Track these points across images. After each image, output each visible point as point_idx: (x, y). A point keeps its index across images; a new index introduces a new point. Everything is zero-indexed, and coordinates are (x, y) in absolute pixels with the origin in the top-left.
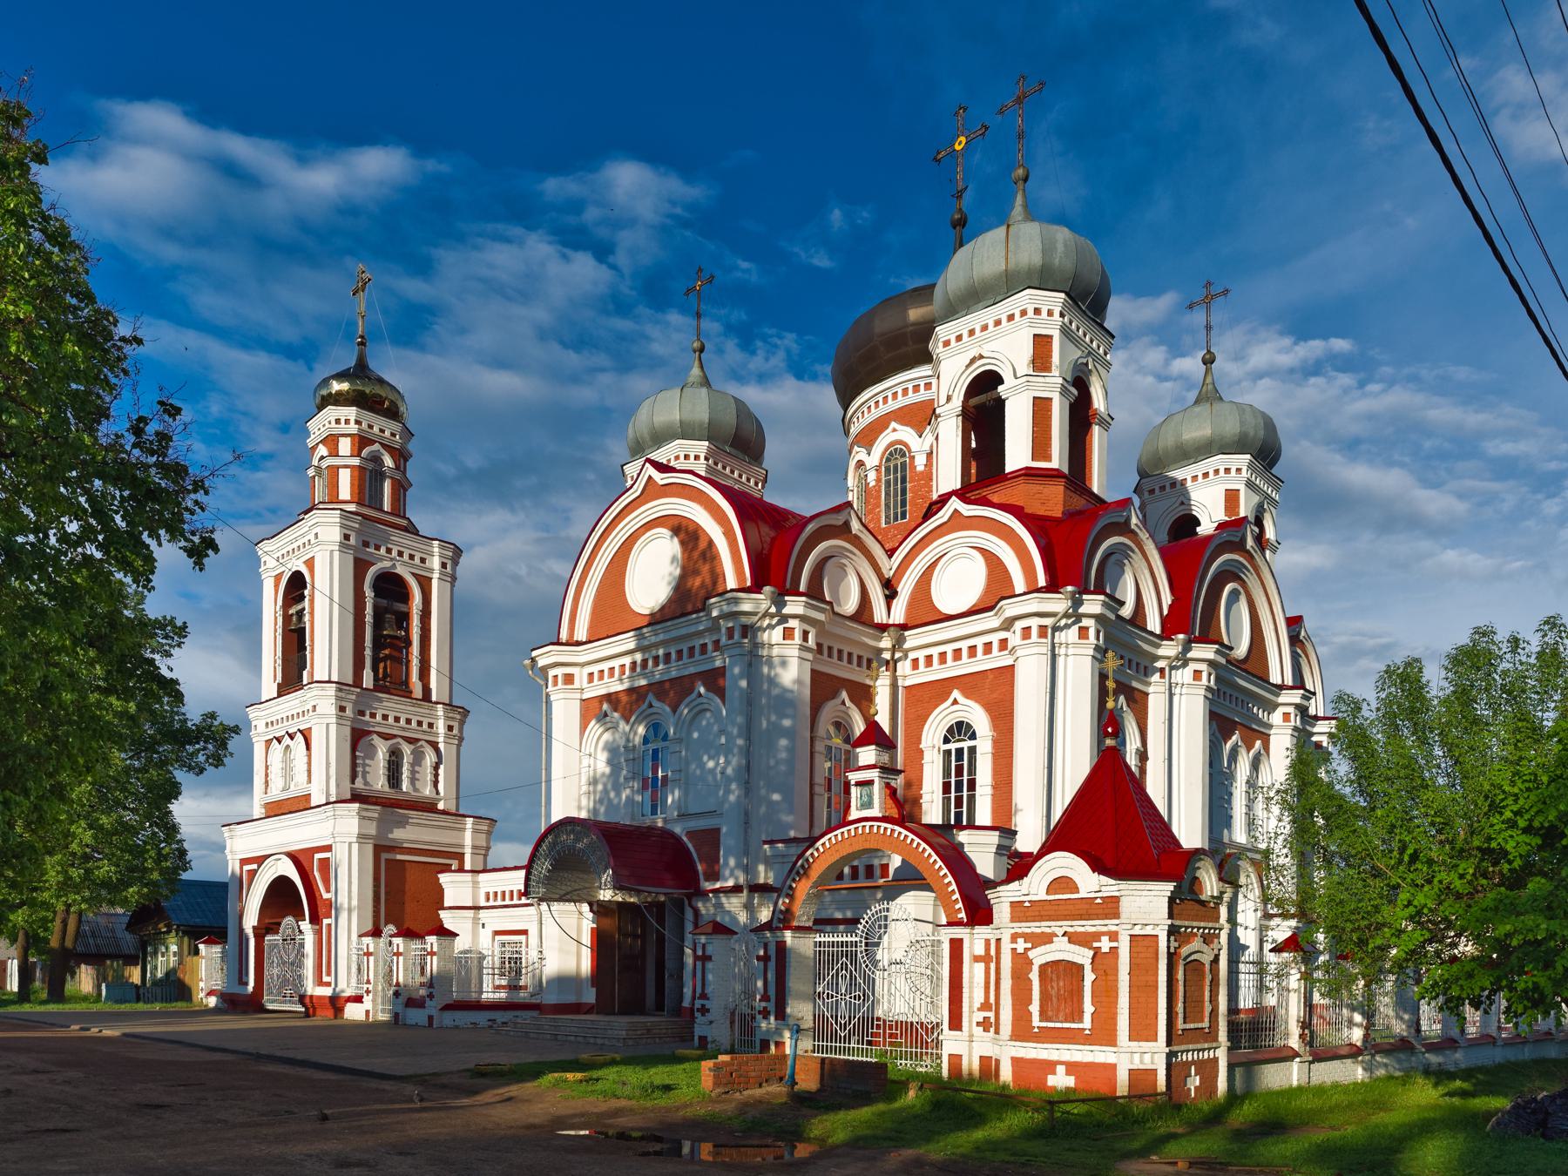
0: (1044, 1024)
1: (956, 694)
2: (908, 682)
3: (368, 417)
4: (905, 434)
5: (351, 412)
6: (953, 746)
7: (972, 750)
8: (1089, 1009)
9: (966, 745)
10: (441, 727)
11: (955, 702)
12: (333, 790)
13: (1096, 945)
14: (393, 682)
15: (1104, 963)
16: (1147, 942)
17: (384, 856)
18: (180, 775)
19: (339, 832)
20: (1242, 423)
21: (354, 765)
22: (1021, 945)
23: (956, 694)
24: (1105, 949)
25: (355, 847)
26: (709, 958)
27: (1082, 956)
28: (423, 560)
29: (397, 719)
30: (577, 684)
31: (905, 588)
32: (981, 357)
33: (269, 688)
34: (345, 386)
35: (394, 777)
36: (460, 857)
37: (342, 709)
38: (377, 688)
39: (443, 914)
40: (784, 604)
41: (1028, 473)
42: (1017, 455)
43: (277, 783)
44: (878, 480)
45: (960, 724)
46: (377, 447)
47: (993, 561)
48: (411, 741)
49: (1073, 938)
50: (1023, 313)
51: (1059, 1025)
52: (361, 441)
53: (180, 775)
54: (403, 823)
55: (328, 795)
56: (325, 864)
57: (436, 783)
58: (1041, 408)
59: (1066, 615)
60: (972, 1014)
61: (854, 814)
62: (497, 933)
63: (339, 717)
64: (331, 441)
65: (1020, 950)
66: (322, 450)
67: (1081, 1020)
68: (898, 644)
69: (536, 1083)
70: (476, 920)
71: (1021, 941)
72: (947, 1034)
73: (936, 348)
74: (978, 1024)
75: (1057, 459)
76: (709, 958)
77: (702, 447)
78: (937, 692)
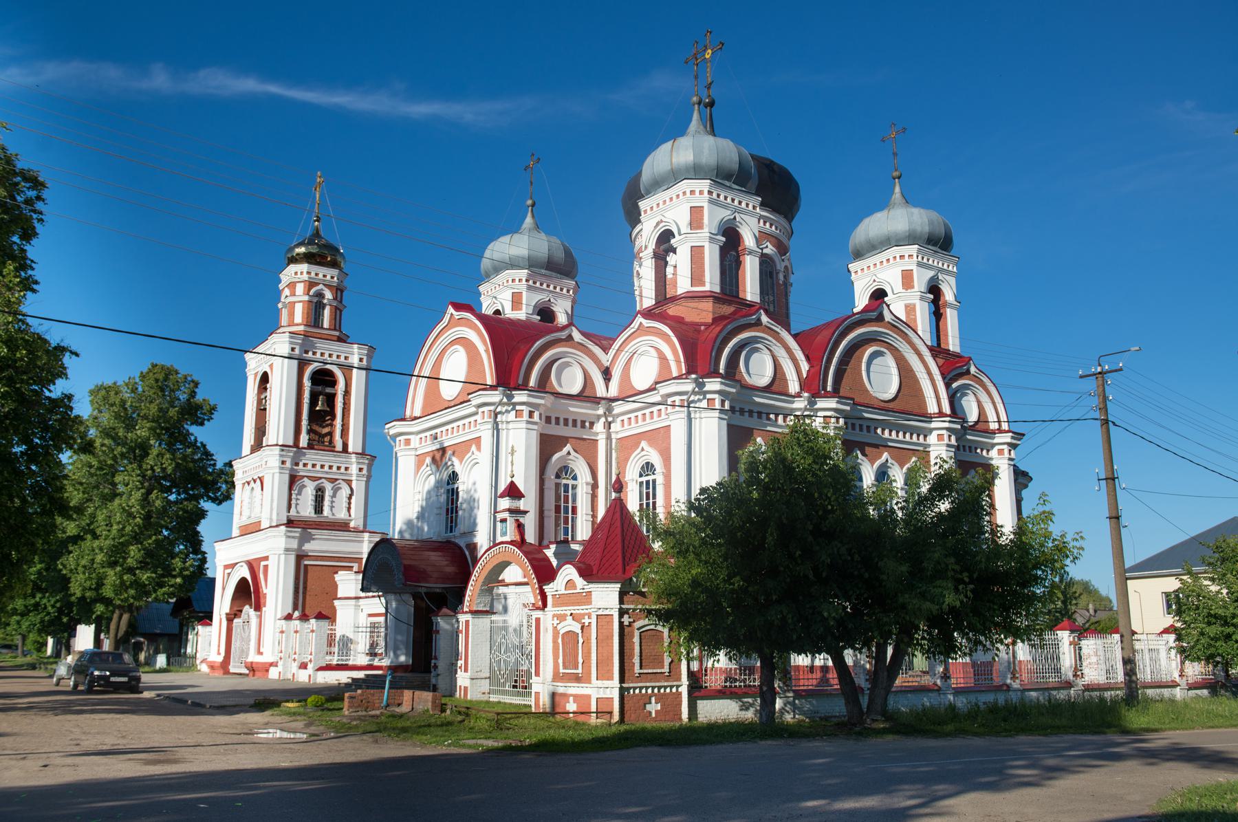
1: (644, 444)
2: (620, 436)
3: (315, 269)
5: (304, 267)
6: (644, 479)
7: (654, 481)
10: (354, 469)
12: (275, 517)
14: (321, 441)
16: (608, 618)
18: (206, 505)
19: (274, 548)
20: (910, 223)
21: (290, 500)
23: (644, 444)
25: (283, 557)
27: (576, 628)
29: (322, 466)
30: (412, 446)
31: (616, 374)
33: (246, 449)
34: (302, 250)
35: (318, 508)
37: (283, 462)
38: (310, 446)
39: (336, 603)
40: (513, 397)
41: (691, 296)
43: (246, 513)
45: (648, 463)
46: (321, 286)
47: (662, 358)
48: (333, 481)
50: (684, 193)
52: (311, 284)
53: (206, 505)
54: (309, 538)
55: (271, 519)
56: (266, 567)
57: (349, 509)
58: (697, 253)
59: (694, 393)
62: (370, 615)
63: (281, 468)
64: (292, 286)
66: (287, 292)
67: (577, 668)
68: (609, 410)
69: (508, 742)
70: (357, 606)
77: (524, 273)
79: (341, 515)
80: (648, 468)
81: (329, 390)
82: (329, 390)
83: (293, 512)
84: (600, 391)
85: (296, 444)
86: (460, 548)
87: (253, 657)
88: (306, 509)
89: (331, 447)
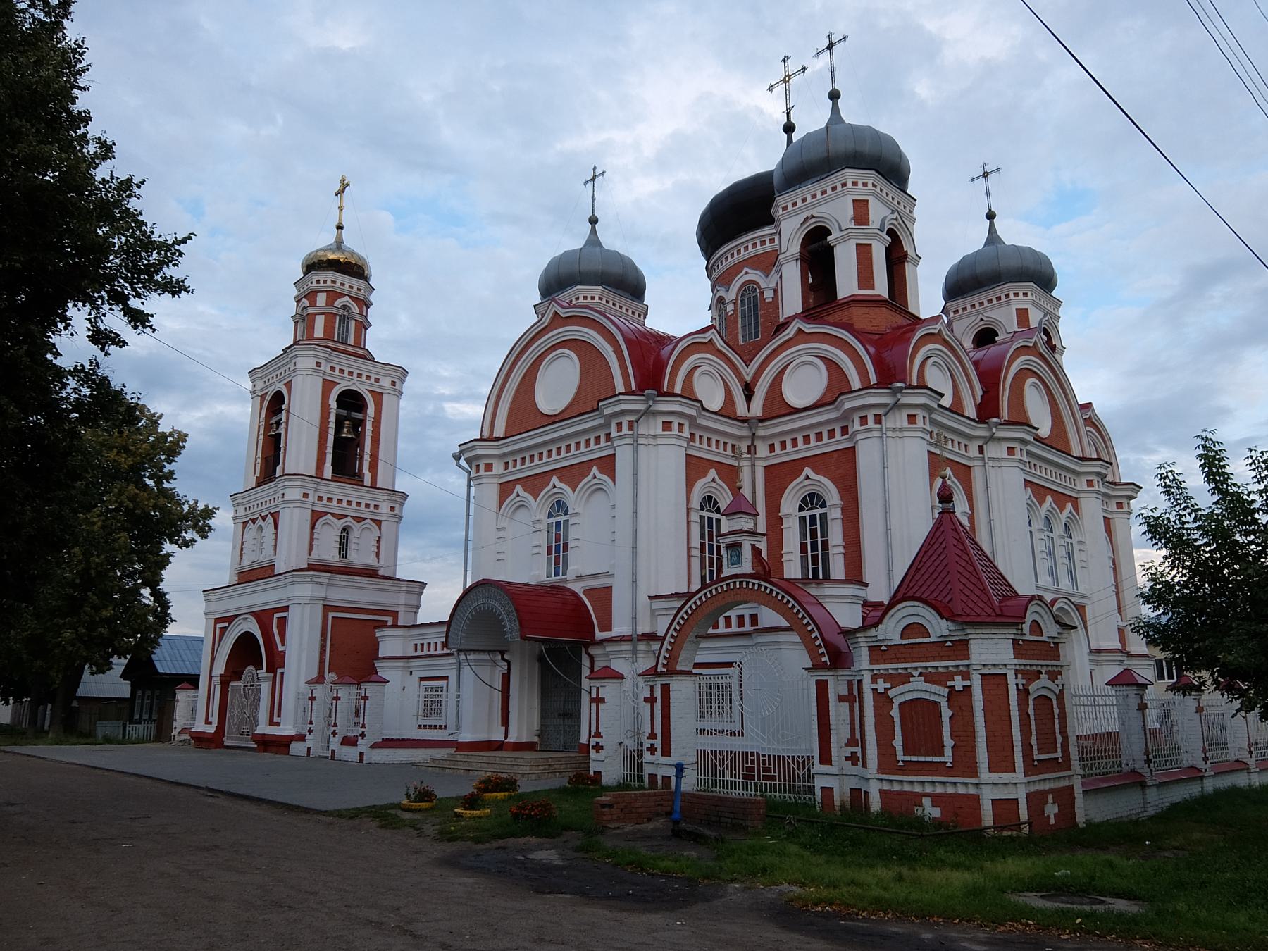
0: (908, 758)
4: (754, 275)
6: (807, 514)
7: (824, 516)
8: (948, 742)
9: (818, 512)
11: (807, 478)
13: (949, 684)
15: (960, 699)
17: (331, 615)
22: (881, 686)
24: (959, 688)
26: (603, 700)
27: (938, 693)
28: (377, 380)
30: (494, 472)
32: (813, 217)
36: (394, 614)
41: (854, 301)
42: (847, 284)
44: (735, 310)
45: (812, 495)
47: (833, 367)
49: (928, 678)
51: (922, 759)
56: (283, 621)
58: (864, 252)
60: (838, 750)
61: (726, 572)
62: (422, 679)
65: (881, 690)
67: (943, 755)
71: (880, 681)
72: (818, 768)
73: (777, 211)
74: (847, 758)
75: (881, 288)
76: (603, 700)
78: (791, 470)
79: (369, 560)
80: (812, 500)
81: (360, 416)
82: (355, 415)
83: (315, 555)
84: (741, 409)
85: (319, 475)
86: (574, 594)
87: (263, 729)
88: (328, 552)
89: (359, 482)
